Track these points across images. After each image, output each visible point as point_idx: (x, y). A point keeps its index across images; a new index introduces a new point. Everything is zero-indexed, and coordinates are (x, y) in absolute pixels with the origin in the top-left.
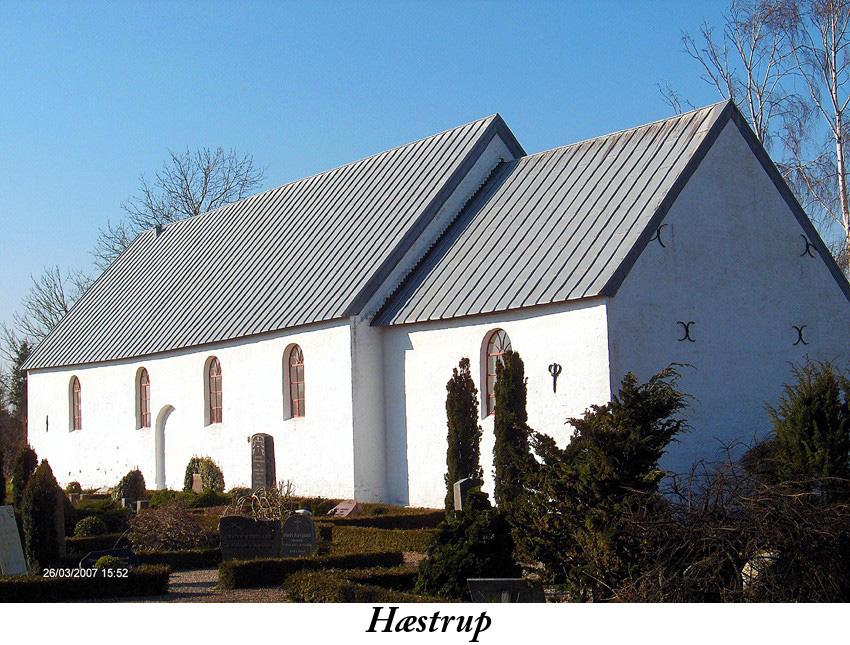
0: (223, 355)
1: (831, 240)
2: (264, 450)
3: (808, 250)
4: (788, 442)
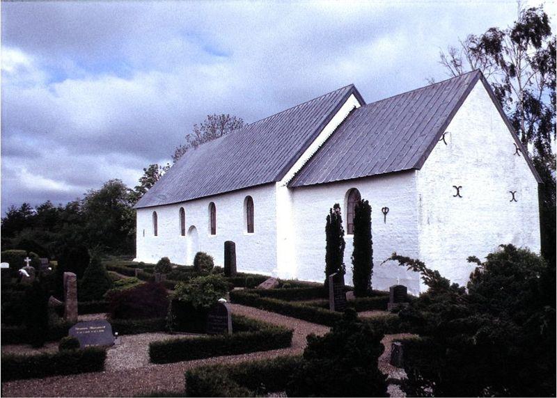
0: (217, 203)
1: (536, 214)
2: (230, 249)
3: (517, 152)
4: (477, 60)
